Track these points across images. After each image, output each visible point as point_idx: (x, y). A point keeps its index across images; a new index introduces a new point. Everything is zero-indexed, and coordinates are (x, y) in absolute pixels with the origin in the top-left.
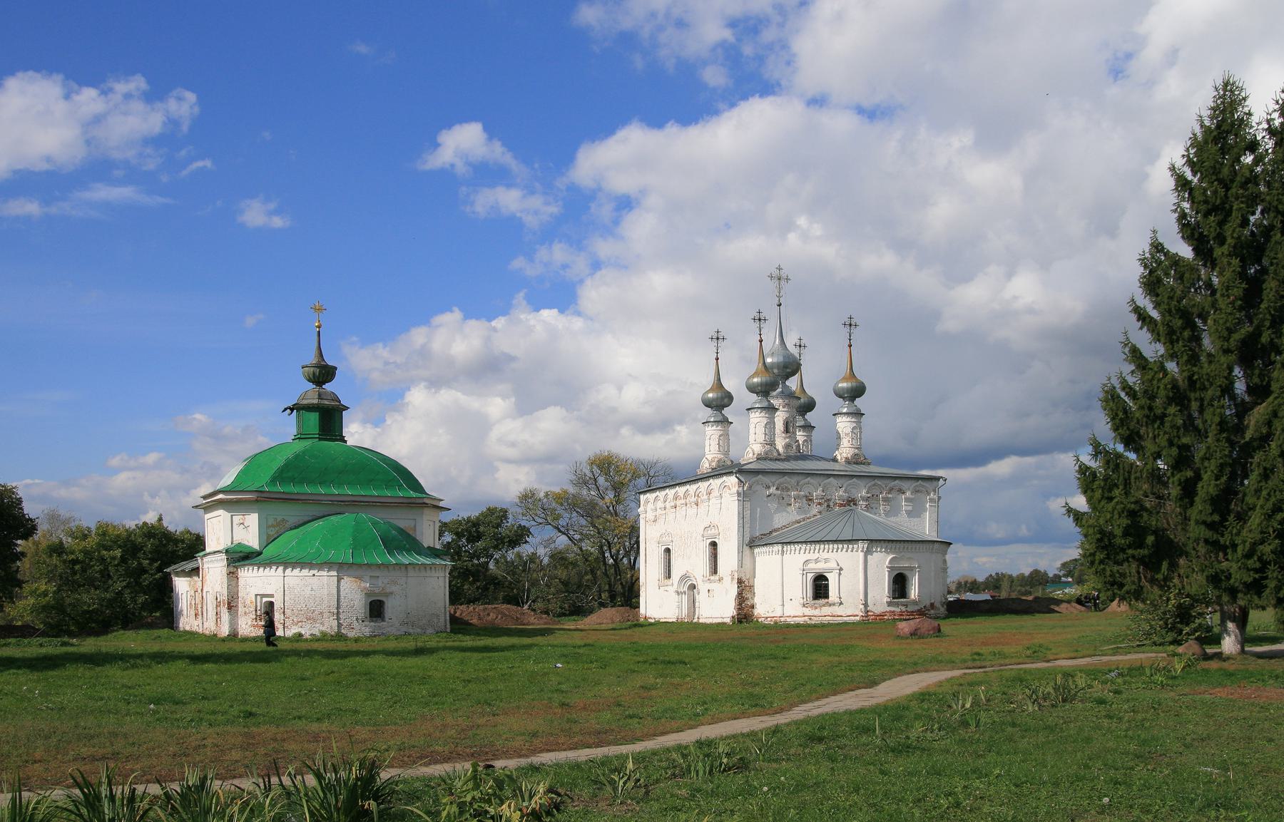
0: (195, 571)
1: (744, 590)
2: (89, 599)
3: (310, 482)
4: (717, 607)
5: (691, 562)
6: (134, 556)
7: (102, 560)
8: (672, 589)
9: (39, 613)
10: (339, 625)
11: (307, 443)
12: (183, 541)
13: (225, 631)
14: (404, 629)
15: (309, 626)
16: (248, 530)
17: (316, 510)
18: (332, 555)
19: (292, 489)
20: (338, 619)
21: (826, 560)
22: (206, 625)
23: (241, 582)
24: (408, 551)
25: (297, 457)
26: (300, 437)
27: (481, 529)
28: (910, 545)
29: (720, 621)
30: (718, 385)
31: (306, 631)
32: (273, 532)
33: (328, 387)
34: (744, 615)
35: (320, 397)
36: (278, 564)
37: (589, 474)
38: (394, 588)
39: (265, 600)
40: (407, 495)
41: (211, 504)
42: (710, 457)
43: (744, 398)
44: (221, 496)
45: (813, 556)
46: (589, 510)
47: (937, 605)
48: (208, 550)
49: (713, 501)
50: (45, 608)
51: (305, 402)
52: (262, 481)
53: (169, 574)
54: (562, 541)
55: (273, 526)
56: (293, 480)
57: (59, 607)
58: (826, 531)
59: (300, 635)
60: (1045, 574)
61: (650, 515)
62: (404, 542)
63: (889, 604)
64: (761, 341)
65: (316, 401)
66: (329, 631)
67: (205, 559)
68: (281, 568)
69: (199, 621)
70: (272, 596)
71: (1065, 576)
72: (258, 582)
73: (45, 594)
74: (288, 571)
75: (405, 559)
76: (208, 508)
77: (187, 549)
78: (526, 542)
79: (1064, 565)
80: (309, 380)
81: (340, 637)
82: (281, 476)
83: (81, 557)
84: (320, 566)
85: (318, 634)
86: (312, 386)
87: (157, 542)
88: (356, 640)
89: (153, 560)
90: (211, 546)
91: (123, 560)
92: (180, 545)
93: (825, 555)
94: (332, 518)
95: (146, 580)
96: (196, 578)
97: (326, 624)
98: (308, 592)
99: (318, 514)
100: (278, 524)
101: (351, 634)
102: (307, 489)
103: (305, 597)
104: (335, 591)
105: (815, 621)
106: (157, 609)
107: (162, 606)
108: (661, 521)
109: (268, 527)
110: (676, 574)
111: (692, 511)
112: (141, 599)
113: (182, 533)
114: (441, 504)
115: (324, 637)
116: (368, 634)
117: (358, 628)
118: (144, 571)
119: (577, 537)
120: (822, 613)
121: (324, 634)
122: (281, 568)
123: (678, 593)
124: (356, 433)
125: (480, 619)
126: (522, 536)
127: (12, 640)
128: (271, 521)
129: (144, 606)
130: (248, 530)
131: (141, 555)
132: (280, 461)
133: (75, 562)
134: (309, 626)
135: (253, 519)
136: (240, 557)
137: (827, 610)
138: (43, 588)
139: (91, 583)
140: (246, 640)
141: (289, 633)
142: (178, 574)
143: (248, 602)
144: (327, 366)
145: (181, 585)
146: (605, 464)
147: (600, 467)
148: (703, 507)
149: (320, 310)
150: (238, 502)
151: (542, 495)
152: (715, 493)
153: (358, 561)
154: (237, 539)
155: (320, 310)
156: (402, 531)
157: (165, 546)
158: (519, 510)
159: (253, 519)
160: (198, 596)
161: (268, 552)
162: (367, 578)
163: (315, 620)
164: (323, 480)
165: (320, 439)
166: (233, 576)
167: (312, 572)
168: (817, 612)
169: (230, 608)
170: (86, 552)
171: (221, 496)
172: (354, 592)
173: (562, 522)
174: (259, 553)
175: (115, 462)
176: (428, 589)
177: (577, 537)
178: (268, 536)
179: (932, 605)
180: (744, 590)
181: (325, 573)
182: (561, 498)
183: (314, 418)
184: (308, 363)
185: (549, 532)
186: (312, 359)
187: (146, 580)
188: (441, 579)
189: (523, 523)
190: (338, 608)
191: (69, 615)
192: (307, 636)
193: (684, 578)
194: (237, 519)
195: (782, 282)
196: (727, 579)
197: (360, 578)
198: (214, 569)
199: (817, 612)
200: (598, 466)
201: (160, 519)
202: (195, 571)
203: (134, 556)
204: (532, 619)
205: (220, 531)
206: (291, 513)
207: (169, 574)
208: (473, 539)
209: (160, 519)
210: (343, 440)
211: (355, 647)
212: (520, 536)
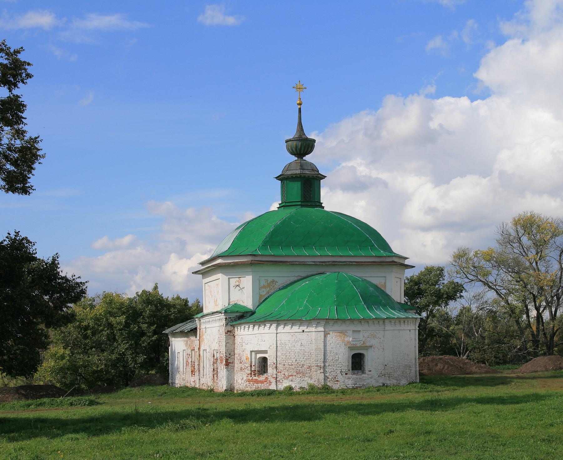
0: (194, 331)
2: (97, 360)
3: (295, 245)
6: (135, 321)
7: (110, 326)
9: (58, 373)
10: (326, 378)
11: (291, 211)
12: (174, 306)
13: (222, 385)
14: (381, 381)
15: (298, 380)
16: (244, 290)
17: (302, 272)
18: (317, 312)
19: (280, 252)
20: (325, 372)
22: (203, 381)
23: (238, 339)
24: (384, 306)
25: (284, 223)
26: (284, 205)
27: (423, 286)
31: (296, 384)
32: (264, 292)
33: (308, 158)
35: (302, 168)
36: (271, 321)
37: (513, 233)
38: (373, 342)
39: (259, 356)
40: (378, 254)
41: (208, 268)
44: (219, 261)
46: (516, 268)
48: (205, 311)
50: (62, 369)
51: (289, 173)
52: (254, 245)
53: (167, 335)
54: (491, 295)
55: (264, 287)
56: (282, 244)
57: (74, 368)
59: (291, 388)
62: (376, 298)
65: (298, 172)
66: (316, 384)
67: (203, 320)
68: (274, 326)
69: (196, 378)
70: (266, 352)
72: (254, 339)
73: (63, 357)
74: (281, 328)
75: (383, 314)
76: (205, 273)
77: (179, 315)
80: (292, 153)
81: (326, 389)
82: (272, 240)
83: (91, 324)
84: (309, 322)
85: (306, 387)
86: (294, 158)
87: (154, 308)
88: (343, 392)
89: (150, 324)
91: (127, 325)
92: (172, 310)
94: (317, 277)
95: (145, 342)
96: (193, 338)
97: (314, 378)
98: (298, 347)
99: (309, 274)
100: (269, 285)
101: (336, 387)
102: (294, 252)
103: (294, 352)
104: (322, 346)
106: (152, 367)
107: (156, 364)
109: (260, 288)
112: (141, 358)
113: (173, 299)
114: (407, 262)
115: (312, 390)
116: (350, 386)
117: (343, 380)
118: (143, 334)
119: (504, 291)
121: (312, 387)
122: (274, 326)
124: (332, 200)
125: (430, 369)
126: (456, 292)
127: (46, 400)
128: (263, 283)
129: (143, 366)
131: (140, 319)
132: (269, 228)
133: (86, 328)
134: (298, 380)
135: (247, 281)
136: (237, 317)
138: (61, 351)
139: (100, 347)
140: (243, 394)
141: (282, 386)
142: (175, 335)
143: (244, 358)
144: (307, 139)
145: (178, 346)
147: (524, 227)
149: (299, 89)
150: (235, 265)
151: (472, 254)
153: (343, 316)
154: (234, 300)
155: (299, 89)
156: (376, 287)
157: (159, 311)
158: (454, 269)
159: (247, 281)
161: (260, 312)
162: (350, 333)
163: (304, 374)
164: (305, 242)
165: (302, 206)
166: (230, 333)
167: (302, 328)
169: (227, 364)
170: (97, 319)
171: (219, 261)
172: (339, 346)
173: (491, 279)
174: (253, 313)
175: (98, 244)
176: (396, 344)
177: (504, 291)
178: (260, 298)
181: (313, 329)
182: (489, 257)
183: (296, 188)
184: (291, 137)
185: (478, 288)
186: (292, 133)
187: (145, 342)
188: (413, 332)
189: (456, 280)
190: (324, 362)
191: (80, 375)
192: (297, 389)
194: (233, 282)
197: (343, 333)
198: (212, 331)
201: (156, 288)
202: (194, 331)
203: (135, 321)
204: (474, 369)
205: (217, 293)
206: (281, 276)
207: (167, 335)
209: (156, 288)
210: (320, 205)
211: (346, 401)
212: (454, 292)
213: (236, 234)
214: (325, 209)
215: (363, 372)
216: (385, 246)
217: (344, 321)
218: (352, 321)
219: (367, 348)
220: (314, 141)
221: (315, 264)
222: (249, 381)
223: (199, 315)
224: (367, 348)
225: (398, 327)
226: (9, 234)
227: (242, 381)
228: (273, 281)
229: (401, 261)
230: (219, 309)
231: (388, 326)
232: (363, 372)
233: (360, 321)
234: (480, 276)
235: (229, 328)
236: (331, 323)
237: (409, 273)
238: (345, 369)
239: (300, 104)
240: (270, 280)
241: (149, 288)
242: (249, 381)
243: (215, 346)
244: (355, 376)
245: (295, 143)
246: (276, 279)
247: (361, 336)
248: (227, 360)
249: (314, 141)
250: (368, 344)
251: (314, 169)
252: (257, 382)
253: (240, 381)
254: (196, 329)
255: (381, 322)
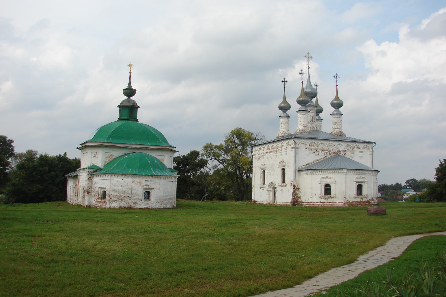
1: (296, 189)
4: (285, 197)
5: (274, 177)
8: (265, 189)
11: (123, 122)
13: (86, 203)
21: (330, 178)
23: (94, 182)
25: (119, 128)
28: (363, 172)
29: (285, 204)
30: (285, 101)
34: (296, 202)
38: (154, 186)
42: (281, 132)
43: (295, 106)
45: (359, 176)
47: (375, 199)
48: (82, 167)
49: (283, 150)
51: (123, 104)
54: (221, 166)
55: (107, 157)
58: (324, 166)
60: (401, 185)
61: (257, 156)
63: (355, 198)
64: (302, 82)
65: (127, 104)
67: (81, 171)
70: (105, 188)
71: (408, 186)
72: (101, 182)
78: (206, 167)
79: (408, 181)
90: (82, 167)
93: (329, 175)
100: (110, 157)
103: (122, 188)
105: (326, 205)
108: (261, 159)
110: (267, 182)
111: (275, 154)
114: (175, 149)
120: (328, 201)
123: (268, 190)
128: (107, 155)
130: (98, 158)
136: (95, 171)
137: (330, 200)
143: (96, 191)
144: (132, 89)
145: (70, 184)
146: (238, 133)
148: (279, 153)
152: (285, 147)
153: (141, 174)
155: (131, 66)
160: (77, 187)
166: (90, 179)
168: (325, 201)
174: (101, 169)
178: (105, 162)
179: (372, 198)
180: (296, 189)
182: (220, 148)
183: (126, 112)
185: (215, 162)
186: (126, 86)
193: (271, 184)
195: (310, 59)
196: (289, 185)
198: (83, 176)
199: (325, 201)
200: (236, 135)
201: (65, 154)
202: (76, 176)
205: (88, 160)
208: (185, 165)
209: (65, 154)
212: (203, 164)
213: (97, 132)
214: (139, 122)
215: (150, 201)
216: (165, 141)
217: (141, 175)
218: (145, 176)
219: (152, 189)
220: (136, 90)
221: (131, 148)
222: (97, 202)
223: (79, 169)
224: (152, 189)
225: (167, 180)
226: (308, 54)
227: (94, 202)
228: (112, 155)
229: (172, 149)
230: (86, 167)
231: (162, 179)
232: (150, 201)
233: (149, 176)
234: (216, 156)
235: (90, 176)
236: (135, 176)
237: (176, 155)
238: (141, 199)
239: (130, 73)
240: (110, 154)
241: (62, 154)
242: (97, 202)
243: (84, 184)
244: (145, 202)
245: (127, 91)
246: (113, 154)
247: (148, 183)
248: (88, 191)
249: (136, 90)
250: (152, 187)
251: (135, 103)
252: (101, 202)
253: (93, 202)
254: (77, 175)
255: (159, 177)
